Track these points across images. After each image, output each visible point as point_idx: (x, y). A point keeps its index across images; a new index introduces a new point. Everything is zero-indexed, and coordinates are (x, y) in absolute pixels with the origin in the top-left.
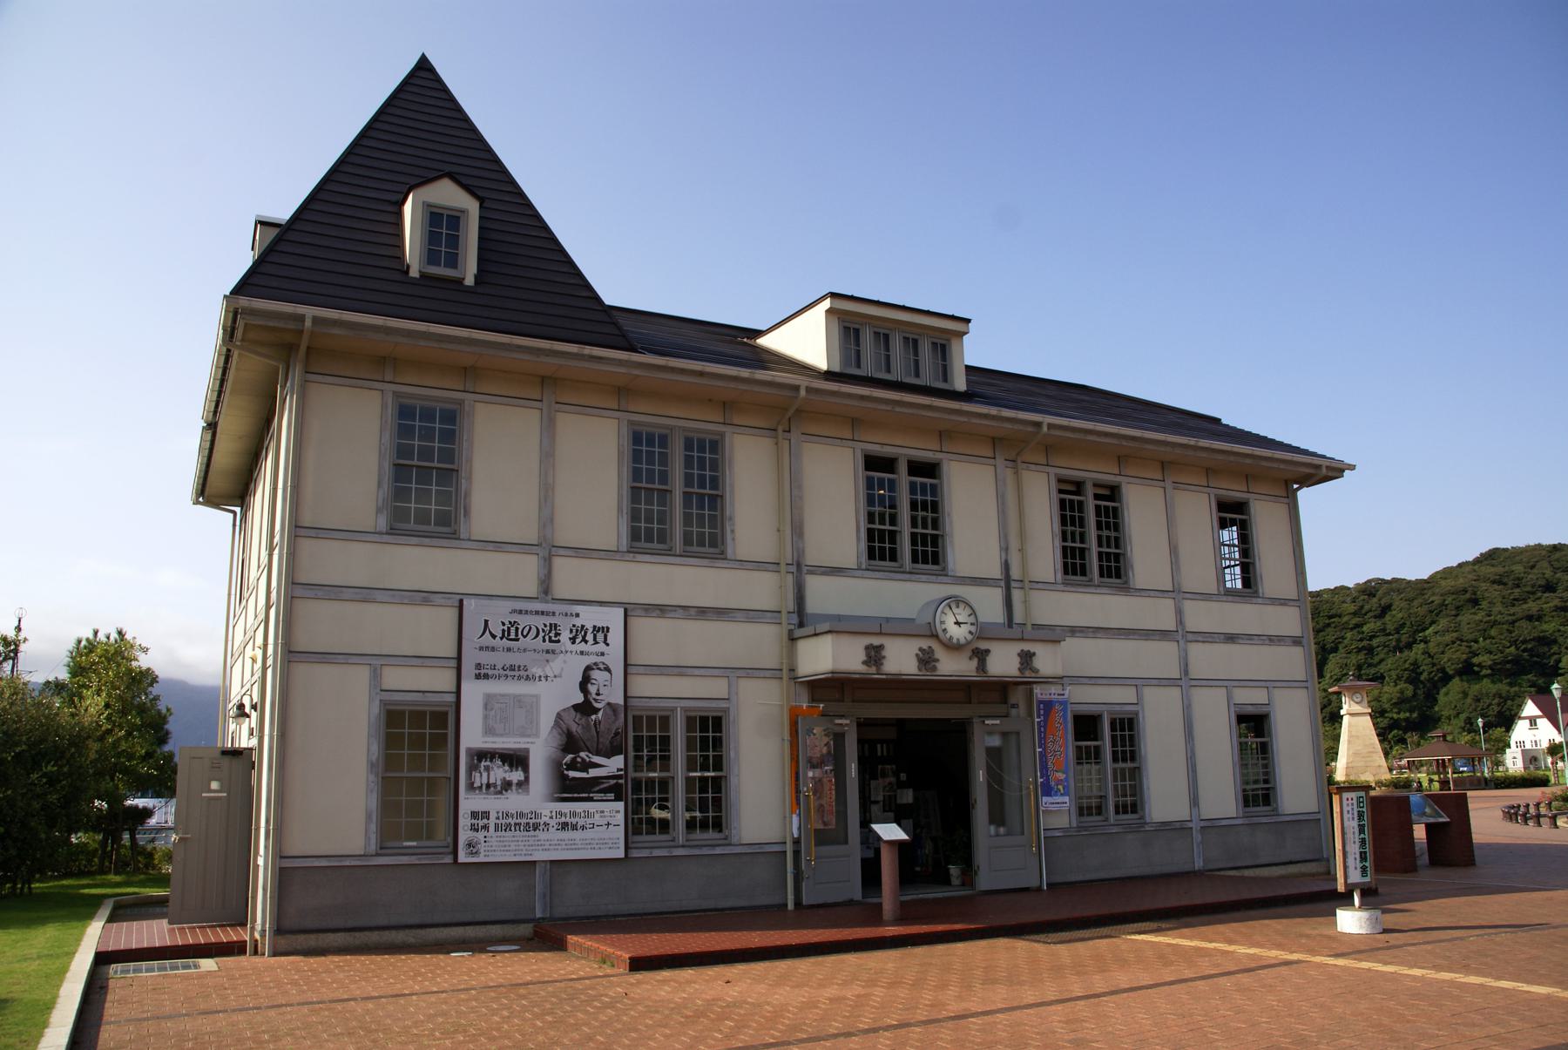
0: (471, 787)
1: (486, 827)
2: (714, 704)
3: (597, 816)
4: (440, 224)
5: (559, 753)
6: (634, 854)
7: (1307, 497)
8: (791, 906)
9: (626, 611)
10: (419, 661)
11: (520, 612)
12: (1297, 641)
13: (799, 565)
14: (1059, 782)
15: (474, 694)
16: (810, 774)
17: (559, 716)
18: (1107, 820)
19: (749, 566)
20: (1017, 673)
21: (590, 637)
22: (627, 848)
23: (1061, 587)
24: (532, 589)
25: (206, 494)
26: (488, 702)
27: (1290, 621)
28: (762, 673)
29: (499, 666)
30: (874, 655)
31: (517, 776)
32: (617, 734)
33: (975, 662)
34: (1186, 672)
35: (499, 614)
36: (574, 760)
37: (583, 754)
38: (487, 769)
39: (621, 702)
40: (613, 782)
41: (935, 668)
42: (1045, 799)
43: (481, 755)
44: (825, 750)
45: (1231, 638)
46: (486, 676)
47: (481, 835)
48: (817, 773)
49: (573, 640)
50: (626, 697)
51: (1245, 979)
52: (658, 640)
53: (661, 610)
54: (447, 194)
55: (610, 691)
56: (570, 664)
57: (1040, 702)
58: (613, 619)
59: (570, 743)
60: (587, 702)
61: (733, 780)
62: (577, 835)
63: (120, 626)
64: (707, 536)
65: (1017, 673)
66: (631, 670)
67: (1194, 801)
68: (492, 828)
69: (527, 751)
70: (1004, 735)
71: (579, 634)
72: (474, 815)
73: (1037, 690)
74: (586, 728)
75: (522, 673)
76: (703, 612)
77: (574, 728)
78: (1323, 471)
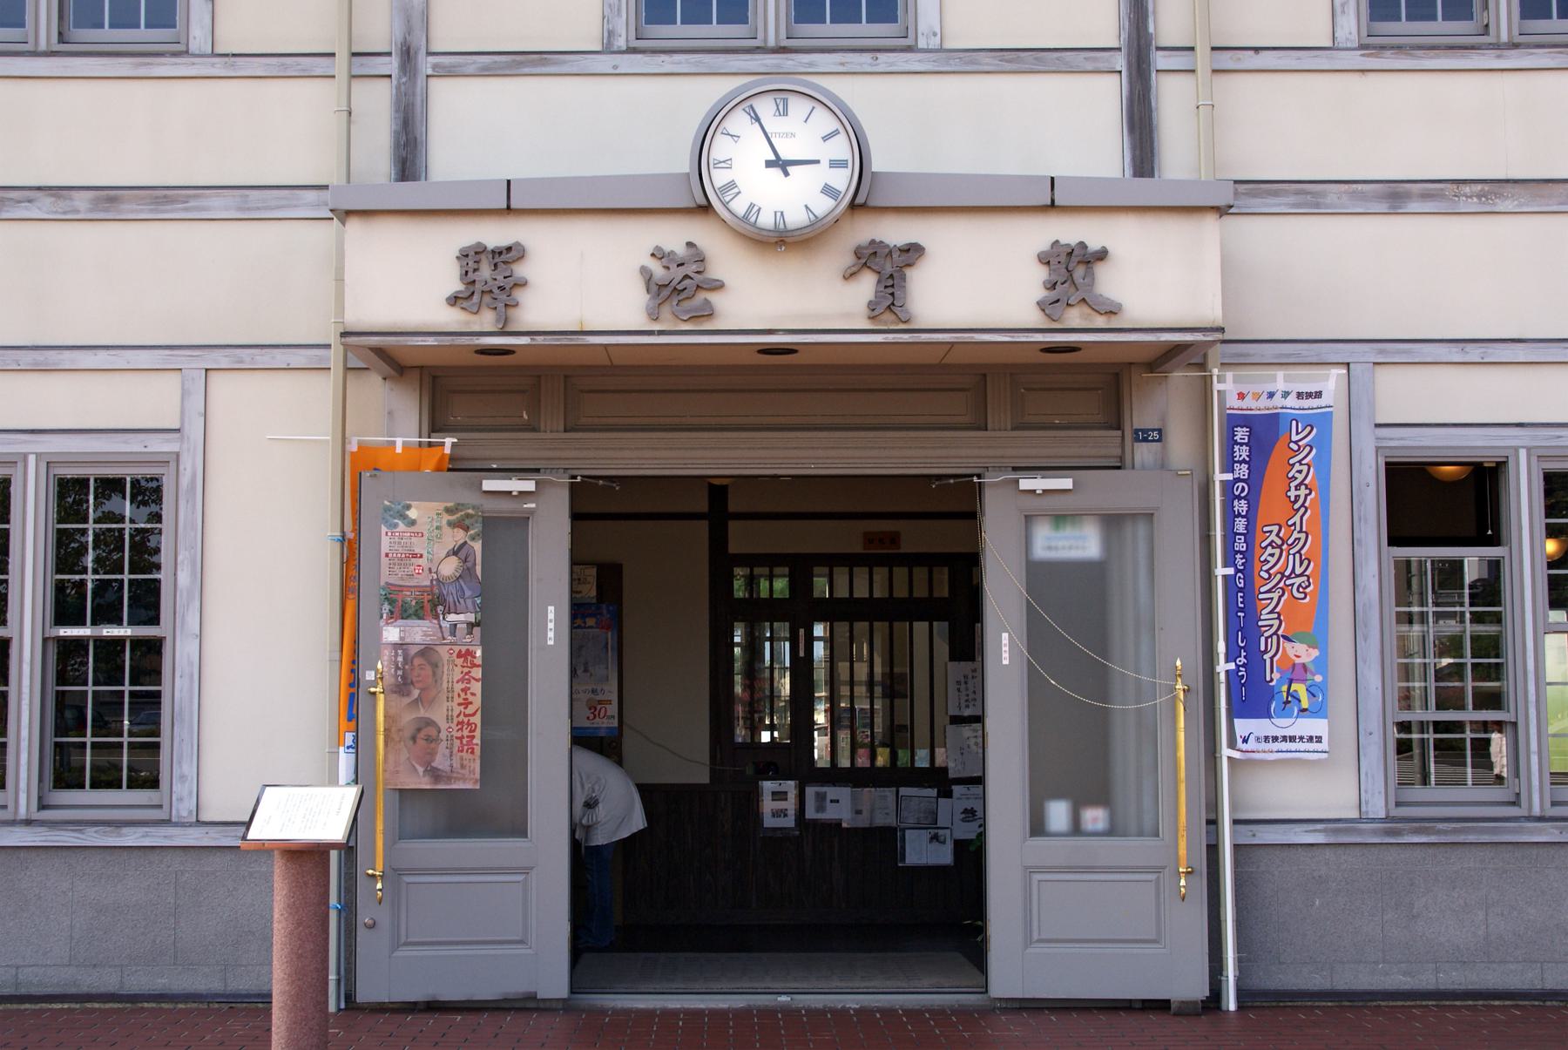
2: (134, 445)
13: (407, 55)
14: (1297, 672)
16: (392, 634)
19: (257, 66)
20: (1033, 318)
23: (1356, 60)
28: (281, 358)
33: (867, 285)
41: (708, 313)
42: (1243, 726)
44: (450, 567)
48: (420, 632)
57: (1233, 421)
65: (1033, 318)
70: (1112, 523)
73: (1228, 388)
76: (110, 201)
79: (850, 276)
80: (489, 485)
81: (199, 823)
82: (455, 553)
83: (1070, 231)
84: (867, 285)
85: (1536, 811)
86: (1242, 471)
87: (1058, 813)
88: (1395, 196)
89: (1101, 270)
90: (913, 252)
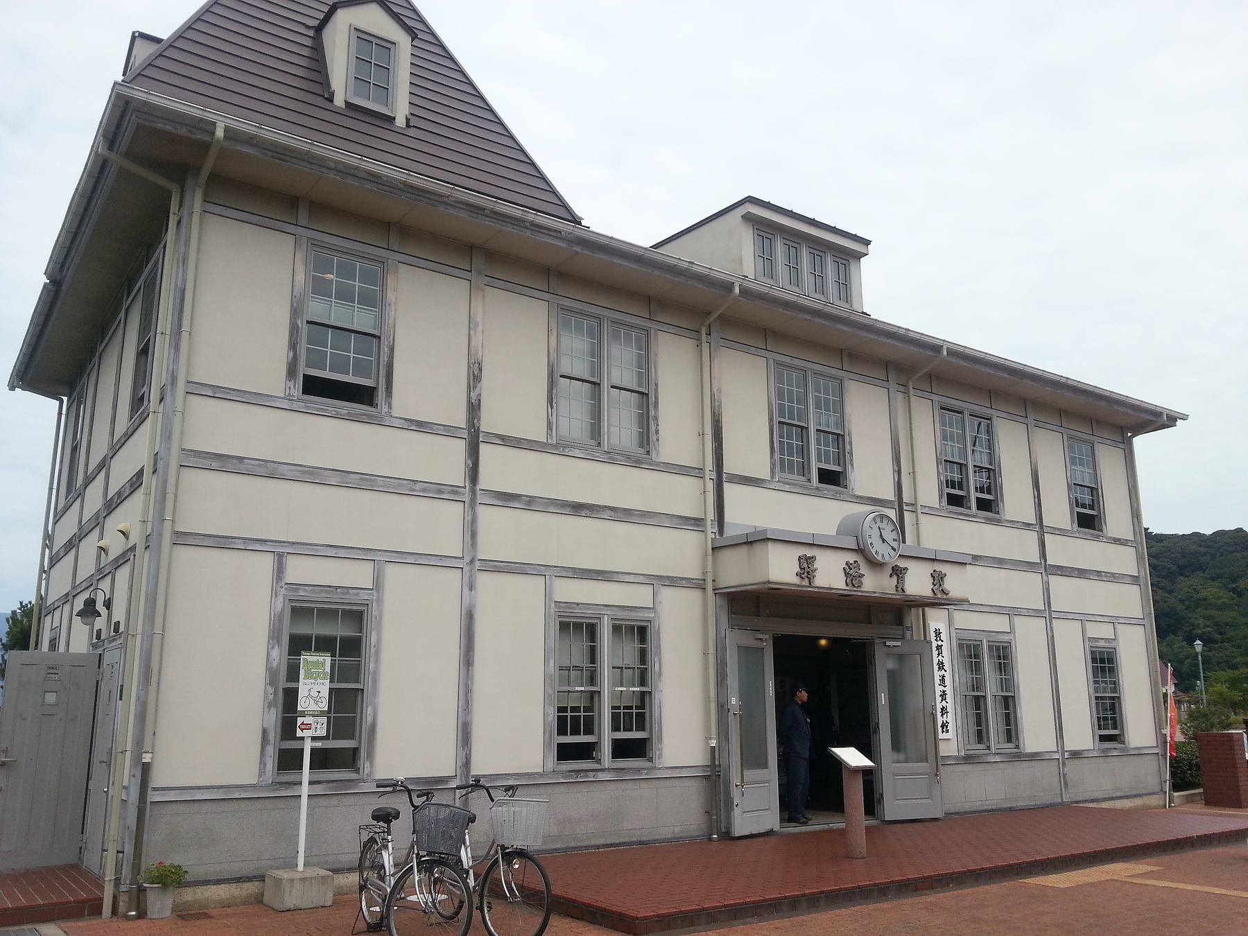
2: (632, 615)
4: (371, 48)
7: (1143, 444)
10: (331, 552)
12: (1135, 580)
18: (988, 748)
20: (930, 594)
25: (35, 372)
27: (1127, 561)
30: (806, 567)
54: (372, 18)
61: (657, 697)
65: (930, 594)
78: (1156, 419)
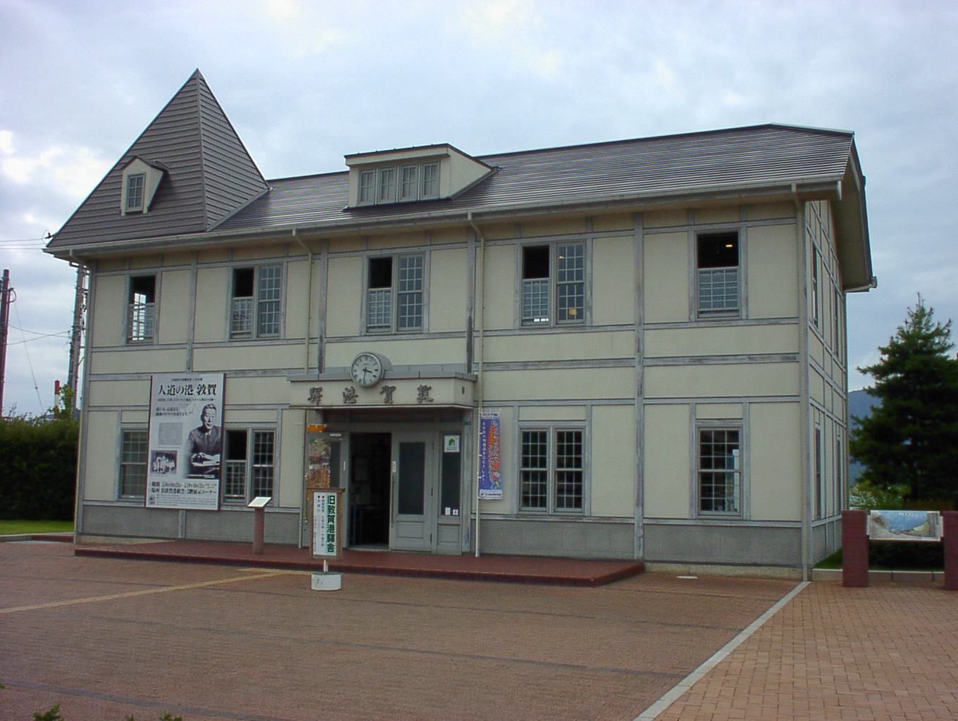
0: (153, 470)
1: (158, 490)
2: (268, 426)
3: (206, 487)
5: (190, 454)
6: (223, 508)
8: (300, 547)
9: (225, 375)
11: (176, 380)
14: (496, 479)
15: (155, 422)
17: (191, 434)
21: (207, 391)
22: (220, 505)
24: (183, 367)
26: (162, 426)
29: (166, 409)
31: (171, 465)
32: (217, 443)
33: (384, 395)
34: (640, 393)
35: (166, 381)
36: (196, 457)
37: (201, 454)
38: (159, 460)
39: (220, 426)
40: (214, 469)
43: (158, 454)
44: (323, 453)
45: (699, 360)
46: (161, 414)
47: (156, 493)
48: (317, 467)
49: (199, 393)
50: (223, 422)
51: (386, 605)
52: (241, 391)
53: (242, 373)
55: (215, 420)
56: (196, 406)
57: (482, 420)
58: (218, 380)
59: (196, 448)
60: (204, 426)
62: (196, 496)
63: (940, 320)
64: (268, 327)
66: (226, 407)
67: (640, 502)
68: (160, 491)
69: (176, 452)
71: (202, 389)
72: (154, 484)
74: (203, 440)
75: (176, 412)
77: (198, 440)
79: (381, 393)
80: (331, 435)
81: (279, 507)
82: (324, 450)
83: (424, 383)
84: (384, 395)
85: (550, 513)
86: (484, 432)
87: (448, 510)
88: (525, 365)
89: (430, 392)
90: (394, 388)
